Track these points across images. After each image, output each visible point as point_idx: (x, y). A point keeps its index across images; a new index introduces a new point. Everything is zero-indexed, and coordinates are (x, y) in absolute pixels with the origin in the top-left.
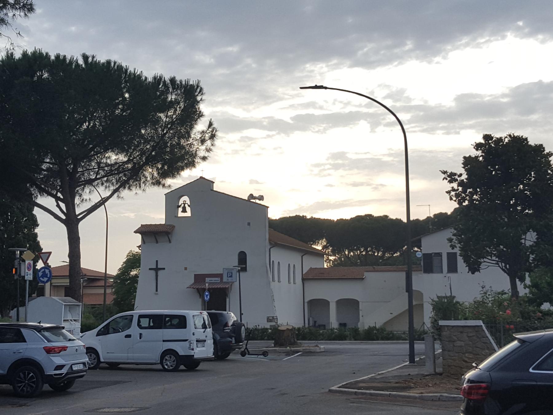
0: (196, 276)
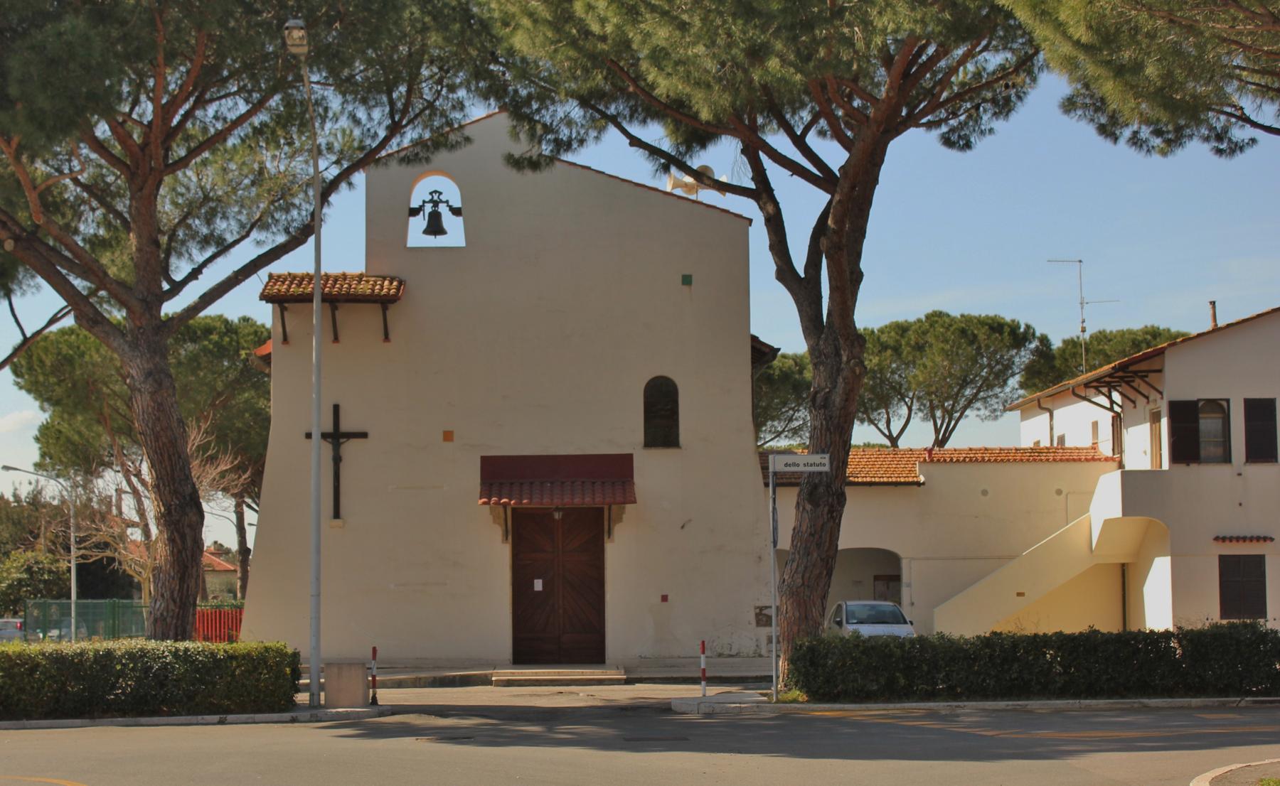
0: (485, 460)
